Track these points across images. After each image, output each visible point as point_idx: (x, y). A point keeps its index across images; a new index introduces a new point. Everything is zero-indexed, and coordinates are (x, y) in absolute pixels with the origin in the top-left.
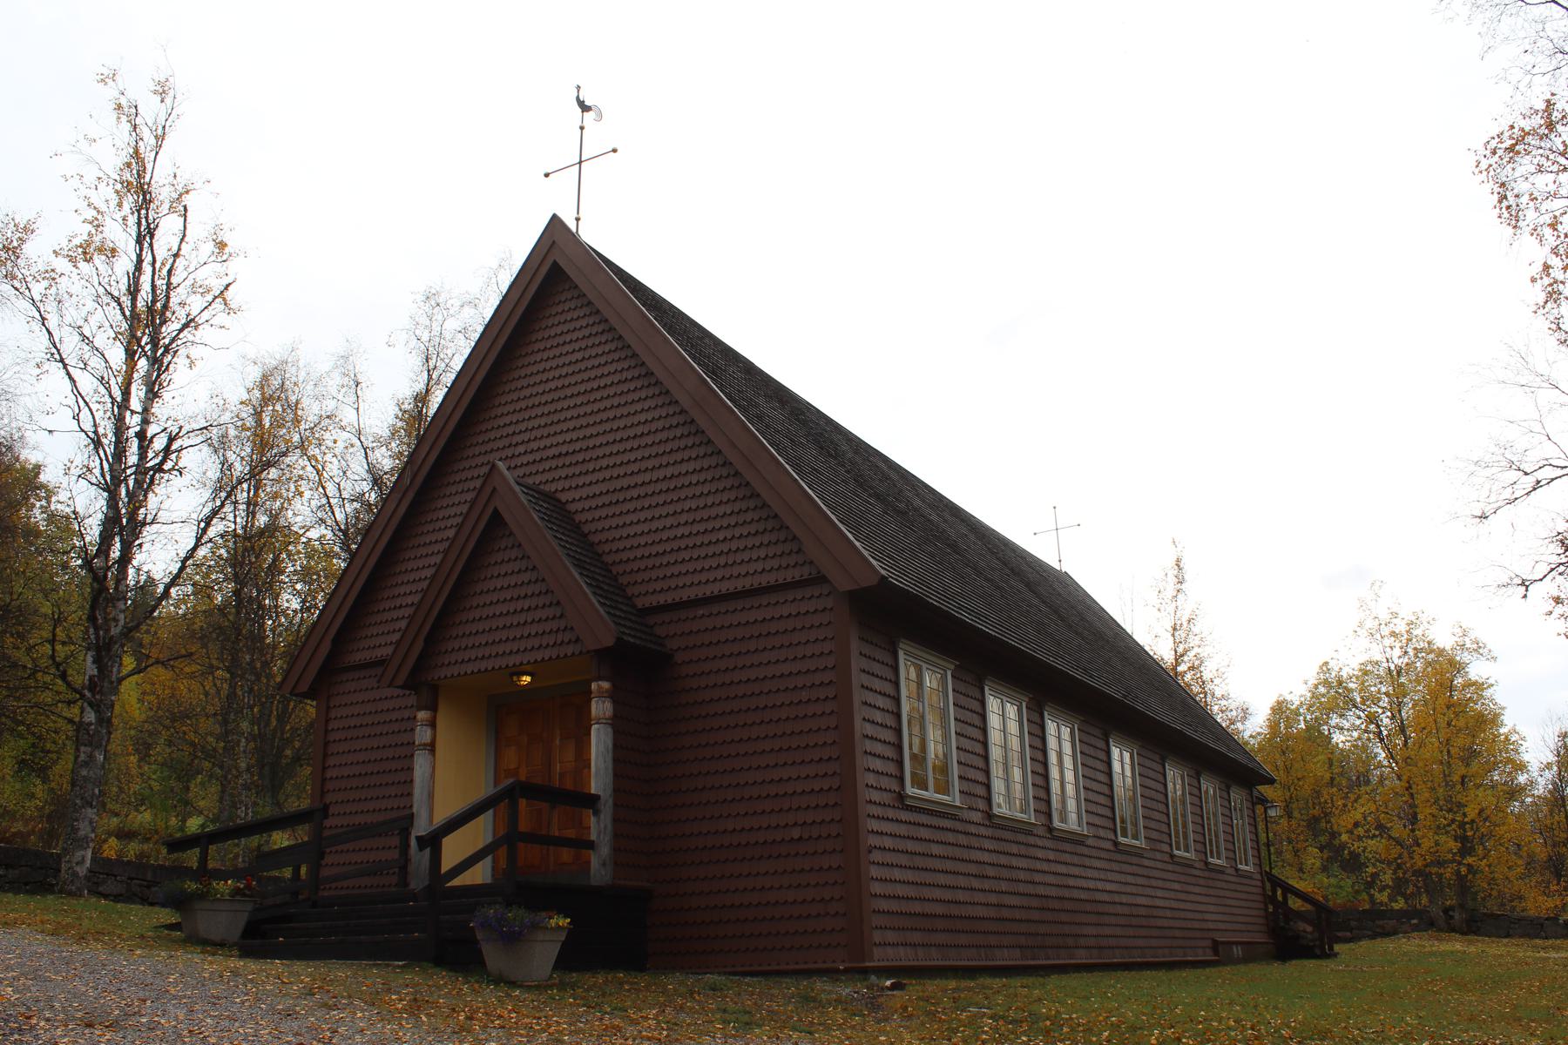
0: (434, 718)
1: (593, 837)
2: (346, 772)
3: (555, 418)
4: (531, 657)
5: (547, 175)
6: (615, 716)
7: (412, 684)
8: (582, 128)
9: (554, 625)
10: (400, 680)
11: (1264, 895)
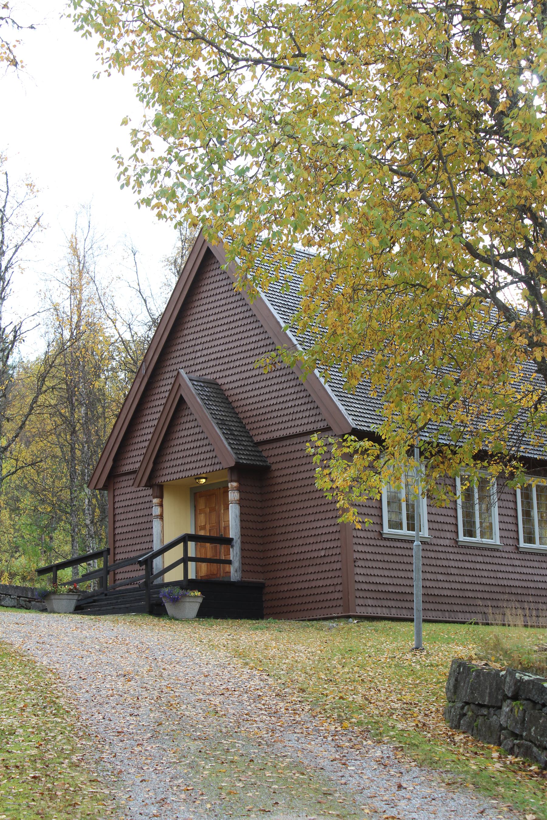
0: (162, 501)
1: (231, 559)
4: (205, 470)
6: (241, 499)
7: (150, 484)
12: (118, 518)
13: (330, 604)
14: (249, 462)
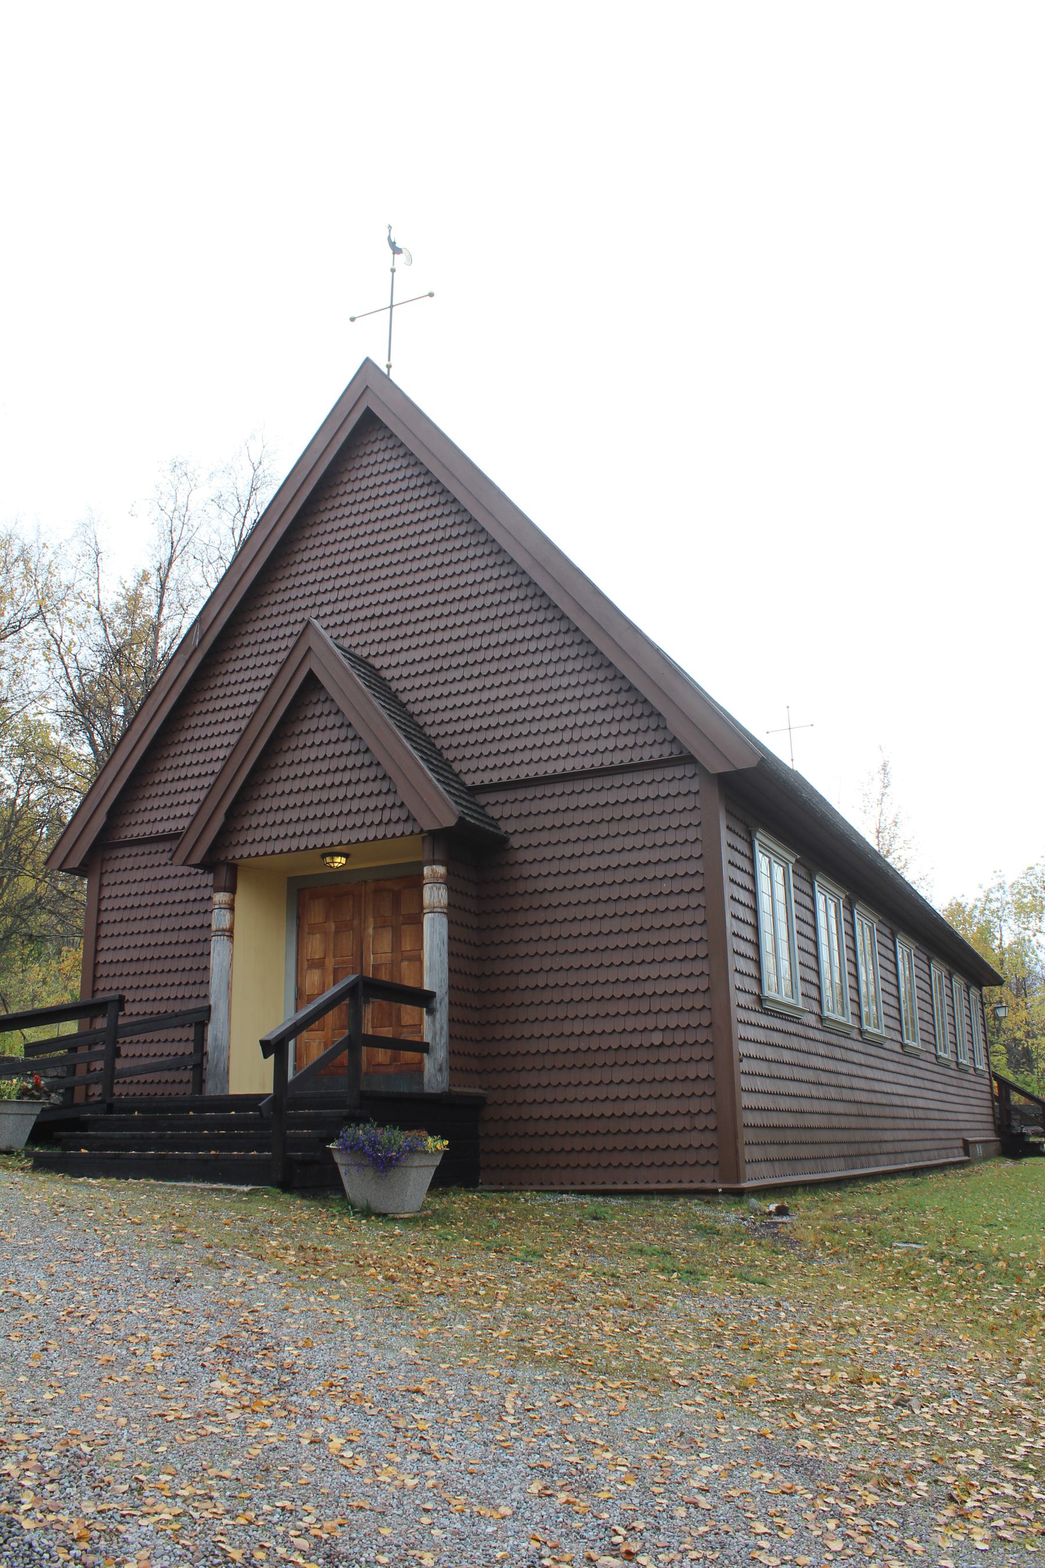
0: (233, 900)
1: (427, 1038)
2: (121, 956)
3: (367, 577)
5: (352, 319)
7: (209, 865)
8: (393, 271)
9: (380, 802)
10: (198, 857)
11: (992, 1093)
12: (105, 930)
13: (679, 1157)
14: (477, 823)
